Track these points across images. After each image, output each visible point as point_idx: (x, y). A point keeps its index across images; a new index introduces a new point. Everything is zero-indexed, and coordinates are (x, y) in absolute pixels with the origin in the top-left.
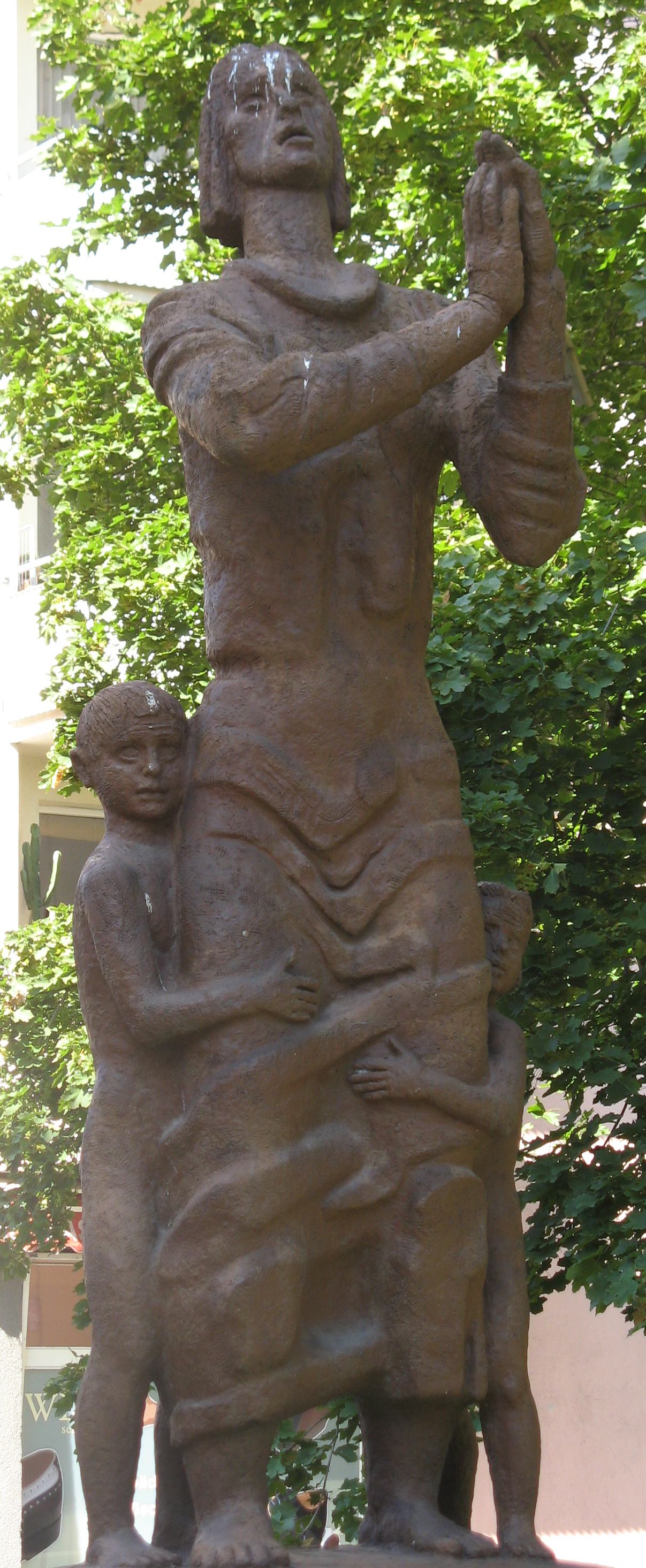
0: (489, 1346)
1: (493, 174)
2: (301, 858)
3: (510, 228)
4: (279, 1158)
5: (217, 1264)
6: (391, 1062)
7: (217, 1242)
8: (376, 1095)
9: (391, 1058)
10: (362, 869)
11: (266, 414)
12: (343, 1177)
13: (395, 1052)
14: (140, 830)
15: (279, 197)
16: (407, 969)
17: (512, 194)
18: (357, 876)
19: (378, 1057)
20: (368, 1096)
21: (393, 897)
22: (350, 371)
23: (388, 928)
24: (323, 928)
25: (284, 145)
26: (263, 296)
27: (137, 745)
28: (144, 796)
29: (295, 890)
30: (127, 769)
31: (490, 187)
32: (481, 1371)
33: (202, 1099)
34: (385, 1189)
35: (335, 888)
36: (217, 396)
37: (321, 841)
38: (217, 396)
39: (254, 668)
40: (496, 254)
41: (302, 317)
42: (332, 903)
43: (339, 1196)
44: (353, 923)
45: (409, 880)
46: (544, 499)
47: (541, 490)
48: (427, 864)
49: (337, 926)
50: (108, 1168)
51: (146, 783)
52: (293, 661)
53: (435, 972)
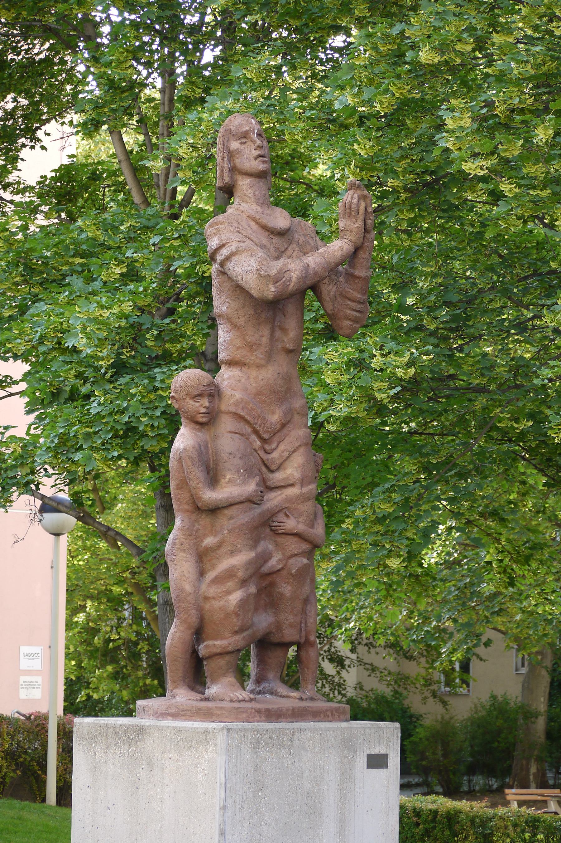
0: (306, 623)
1: (356, 196)
2: (258, 443)
3: (361, 217)
4: (253, 554)
5: (229, 592)
6: (285, 520)
7: (230, 584)
8: (280, 532)
9: (285, 518)
10: (277, 446)
11: (278, 284)
12: (266, 562)
13: (287, 516)
14: (197, 427)
15: (253, 180)
16: (292, 485)
17: (363, 204)
18: (275, 449)
19: (281, 517)
20: (277, 532)
21: (288, 457)
22: (306, 268)
23: (285, 469)
24: (264, 469)
25: (257, 161)
26: (252, 223)
27: (201, 395)
28: (202, 415)
29: (255, 453)
30: (197, 404)
31: (355, 201)
32: (304, 633)
33: (226, 532)
34: (280, 566)
35: (266, 452)
36: (260, 275)
37: (266, 436)
38: (260, 275)
39: (243, 368)
40: (355, 226)
41: (267, 233)
42: (268, 460)
43: (265, 569)
44: (273, 467)
45: (294, 451)
46: (357, 314)
47: (357, 311)
48: (300, 446)
49: (266, 466)
50: (184, 555)
51: (204, 410)
52: (259, 367)
53: (302, 486)
